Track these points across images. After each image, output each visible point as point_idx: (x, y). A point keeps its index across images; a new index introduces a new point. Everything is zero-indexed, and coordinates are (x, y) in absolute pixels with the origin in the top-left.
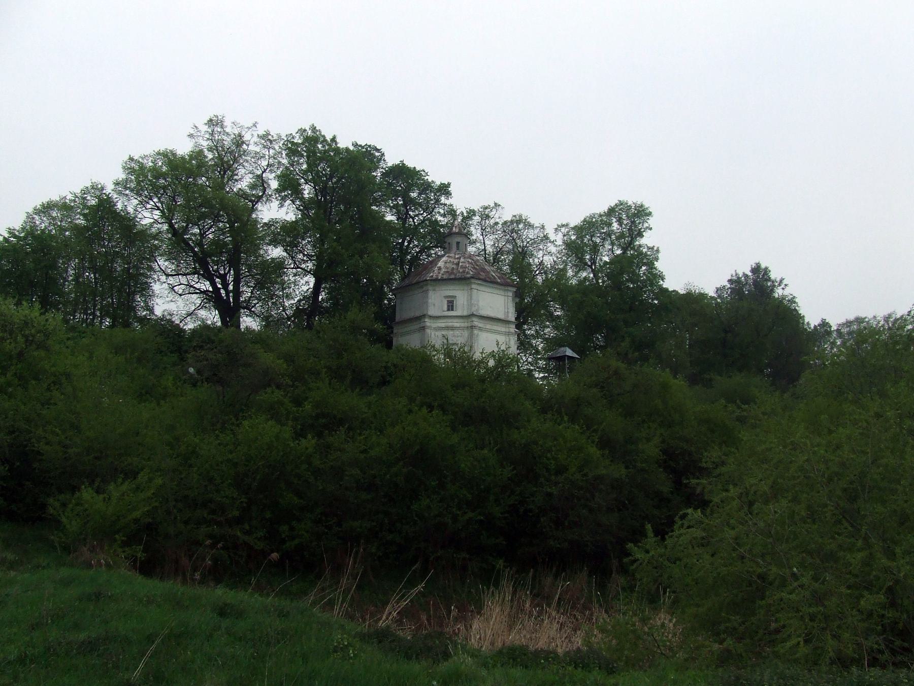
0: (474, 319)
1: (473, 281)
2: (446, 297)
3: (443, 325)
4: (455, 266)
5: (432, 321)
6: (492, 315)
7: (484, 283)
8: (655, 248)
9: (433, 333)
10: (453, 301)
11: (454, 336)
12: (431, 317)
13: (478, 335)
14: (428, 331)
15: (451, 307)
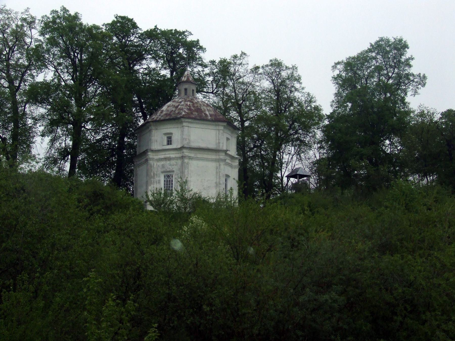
0: (185, 151)
1: (183, 120)
2: (165, 134)
3: (162, 157)
4: (174, 109)
5: (154, 154)
6: (203, 145)
7: (192, 121)
8: (422, 76)
9: (155, 164)
10: (171, 137)
11: (170, 165)
12: (152, 151)
13: (188, 164)
14: (151, 162)
15: (169, 142)
